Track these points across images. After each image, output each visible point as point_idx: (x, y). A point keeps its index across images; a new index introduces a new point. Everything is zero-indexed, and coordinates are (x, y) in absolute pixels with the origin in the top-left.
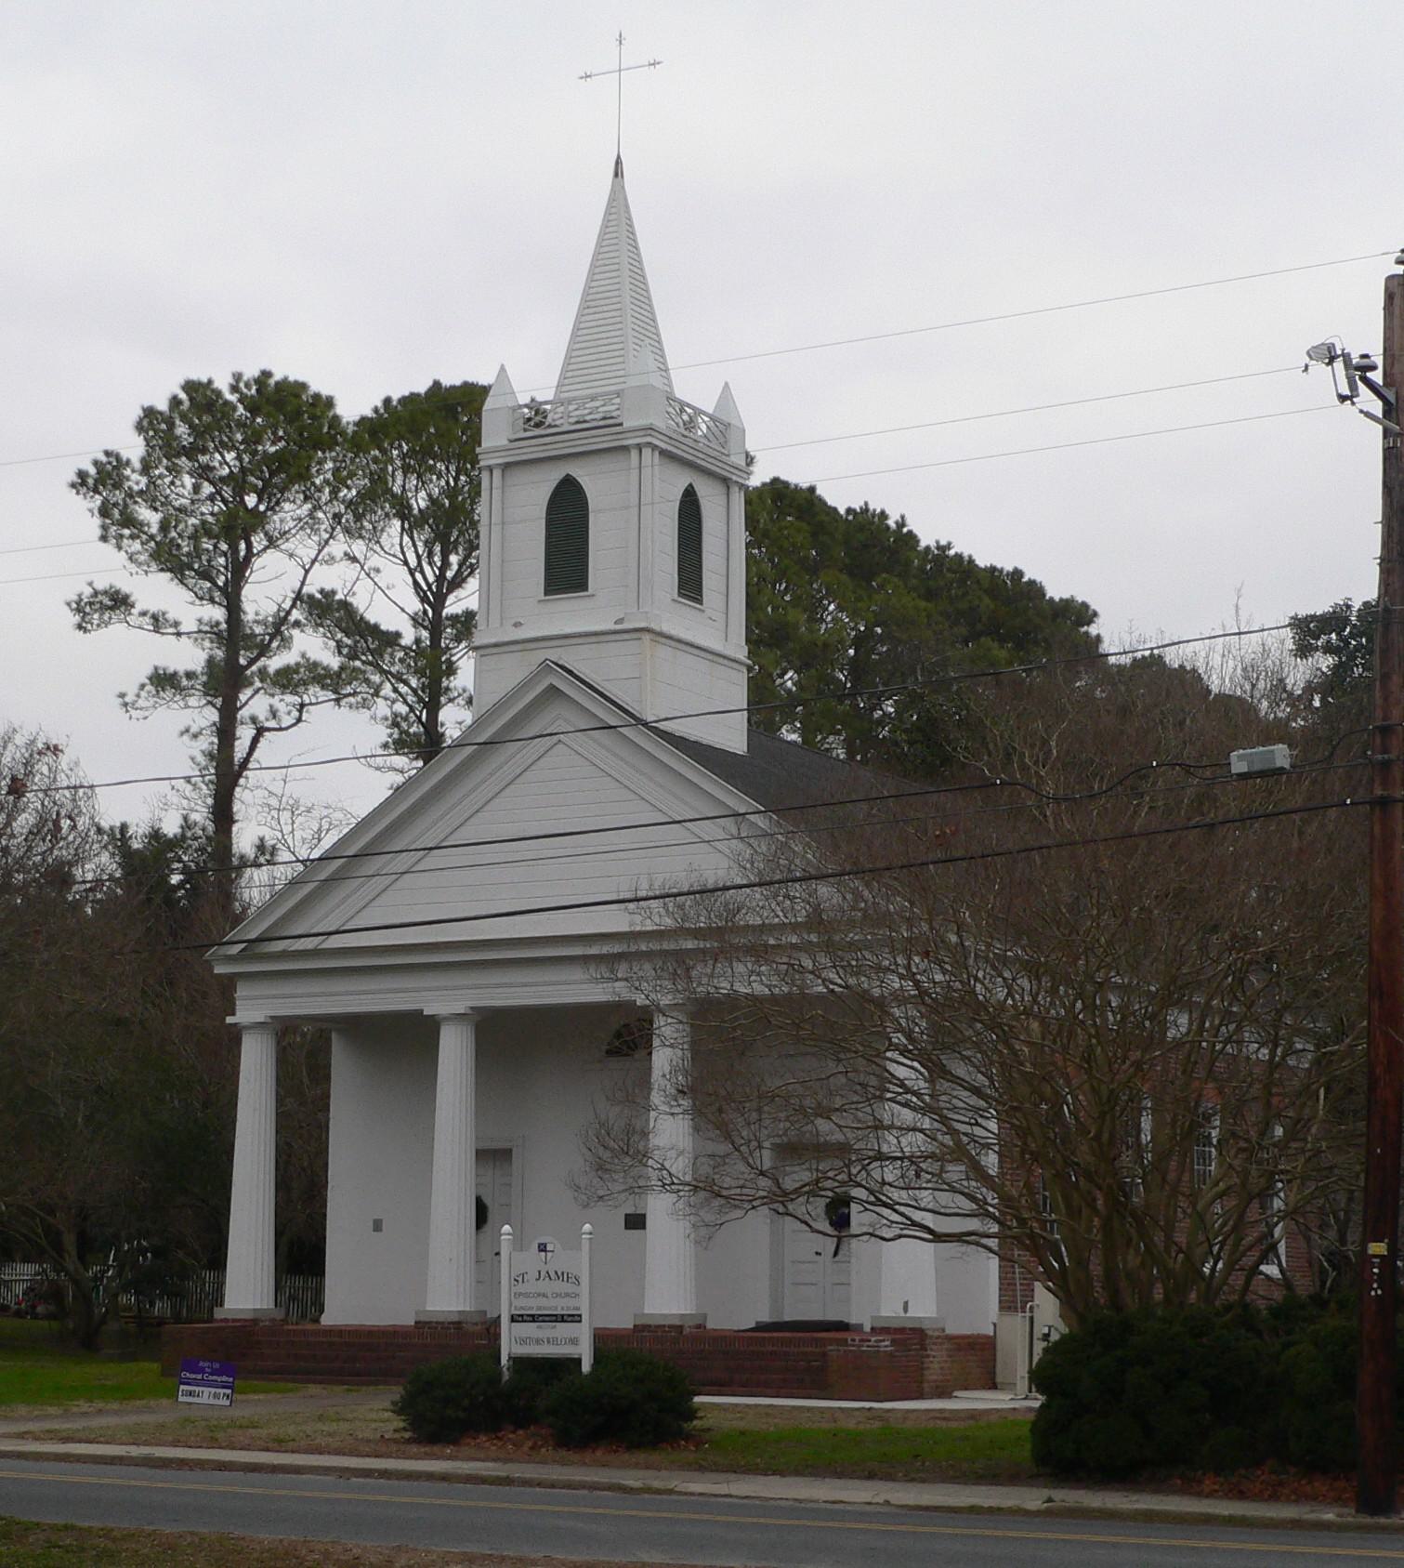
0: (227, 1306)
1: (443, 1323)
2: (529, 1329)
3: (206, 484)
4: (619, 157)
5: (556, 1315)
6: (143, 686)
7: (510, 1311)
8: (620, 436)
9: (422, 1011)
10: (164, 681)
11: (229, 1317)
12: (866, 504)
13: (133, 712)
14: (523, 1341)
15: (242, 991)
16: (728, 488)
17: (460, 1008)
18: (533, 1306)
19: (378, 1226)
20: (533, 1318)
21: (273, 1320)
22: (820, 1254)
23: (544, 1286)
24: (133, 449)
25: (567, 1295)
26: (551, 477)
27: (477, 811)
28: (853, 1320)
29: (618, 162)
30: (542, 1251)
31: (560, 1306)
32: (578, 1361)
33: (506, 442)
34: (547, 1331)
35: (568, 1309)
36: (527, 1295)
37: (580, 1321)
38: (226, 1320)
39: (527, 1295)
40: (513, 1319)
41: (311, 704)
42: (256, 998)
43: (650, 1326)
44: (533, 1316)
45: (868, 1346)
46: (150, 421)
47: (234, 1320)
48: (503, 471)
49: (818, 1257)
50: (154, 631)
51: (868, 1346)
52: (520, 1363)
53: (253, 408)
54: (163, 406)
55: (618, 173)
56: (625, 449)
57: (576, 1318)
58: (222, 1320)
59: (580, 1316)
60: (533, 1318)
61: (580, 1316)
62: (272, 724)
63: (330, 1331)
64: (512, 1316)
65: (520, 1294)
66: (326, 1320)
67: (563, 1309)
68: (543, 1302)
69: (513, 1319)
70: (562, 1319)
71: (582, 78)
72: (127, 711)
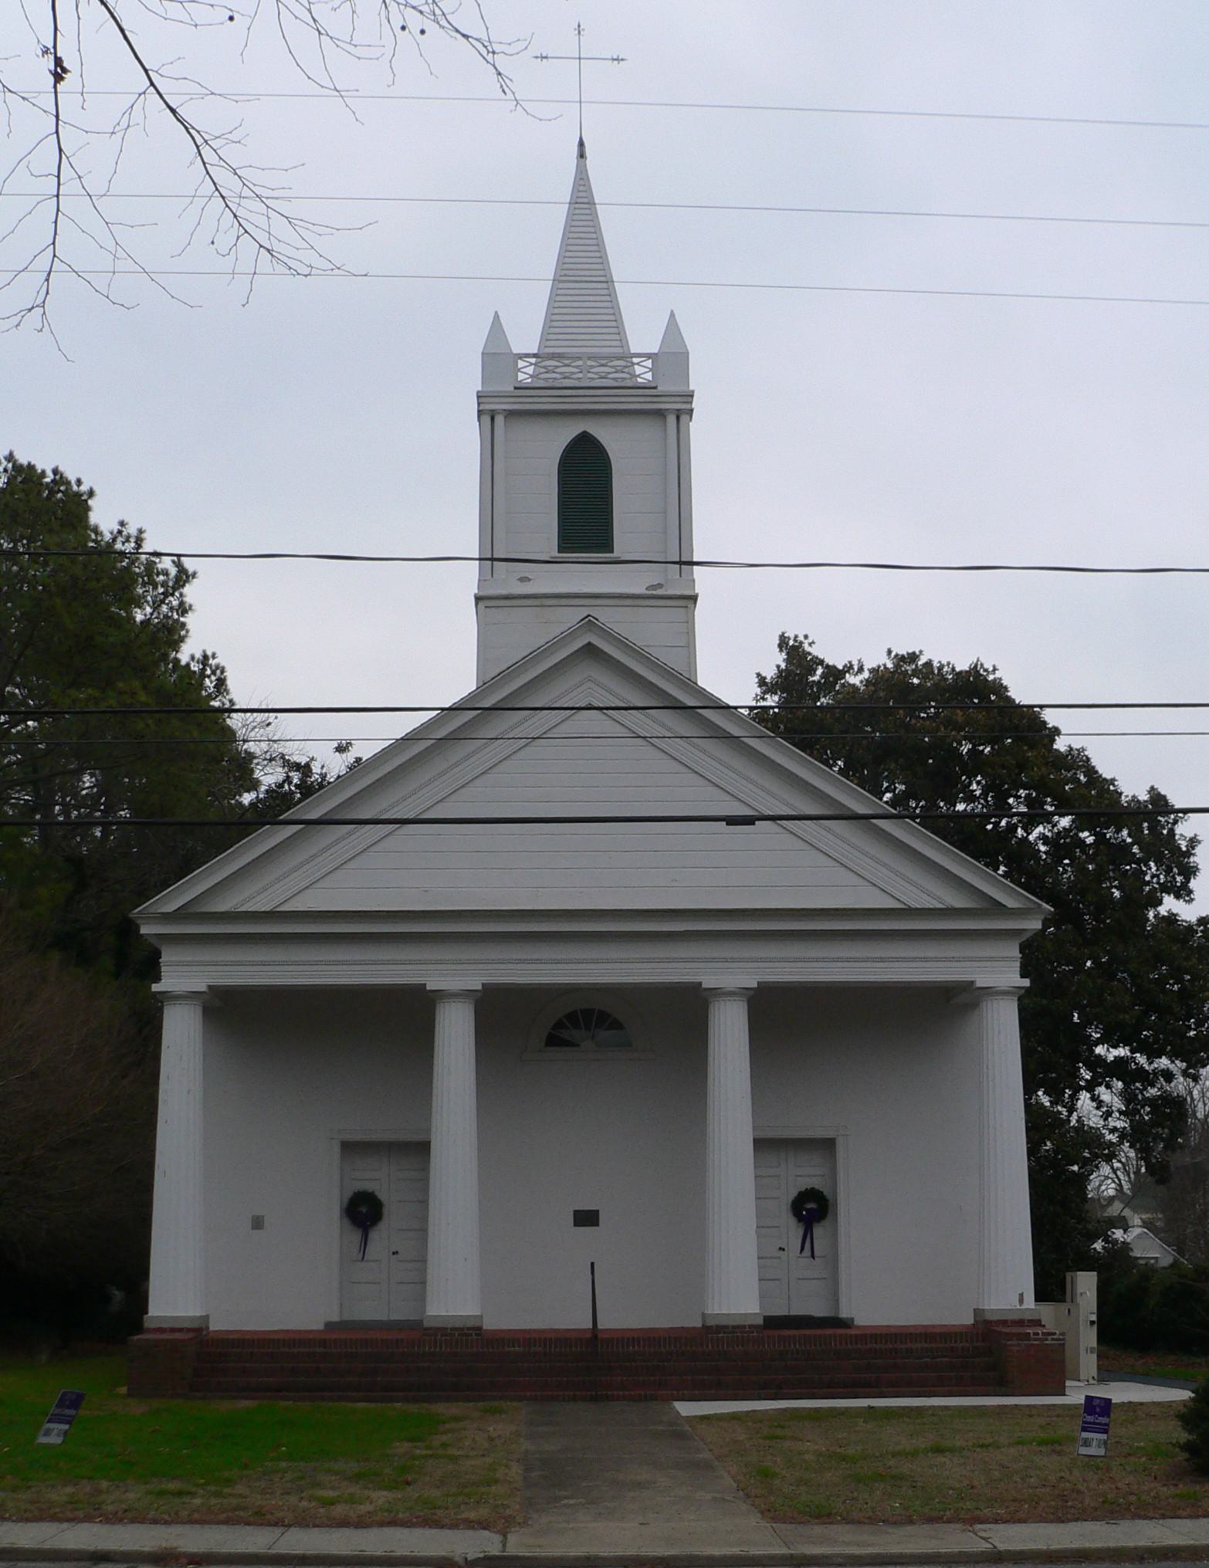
8: (656, 399)
12: (204, 651)
15: (167, 956)
19: (258, 1223)
22: (784, 1250)
26: (564, 434)
28: (844, 1314)
29: (581, 144)
33: (513, 389)
42: (189, 964)
43: (726, 1327)
45: (1053, 1339)
48: (505, 417)
49: (782, 1252)
51: (1053, 1339)
55: (582, 155)
56: (661, 414)
71: (537, 57)
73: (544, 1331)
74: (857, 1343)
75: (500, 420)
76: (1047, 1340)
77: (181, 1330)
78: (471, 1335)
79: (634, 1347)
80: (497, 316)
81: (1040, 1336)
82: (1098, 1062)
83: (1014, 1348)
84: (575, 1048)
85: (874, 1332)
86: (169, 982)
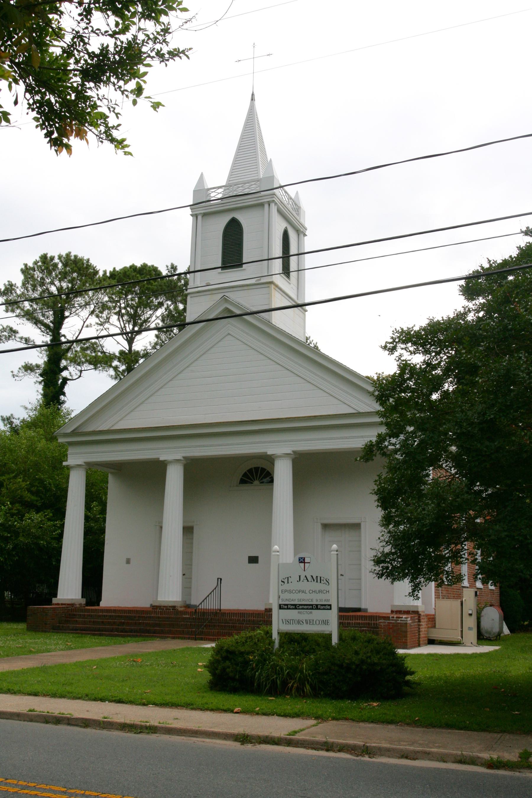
0: (59, 597)
1: (167, 607)
2: (293, 614)
3: (89, 109)
4: (253, 92)
5: (312, 605)
6: (20, 369)
7: (278, 602)
9: (159, 458)
10: (28, 368)
11: (60, 602)
13: (16, 378)
14: (288, 622)
15: (71, 451)
16: (298, 235)
17: (179, 456)
18: (296, 598)
19: (128, 561)
20: (295, 607)
21: (80, 604)
23: (304, 585)
24: (18, 279)
25: (320, 591)
26: (224, 220)
27: (188, 367)
28: (363, 607)
30: (301, 562)
31: (316, 599)
32: (329, 637)
34: (305, 615)
35: (321, 600)
36: (290, 592)
37: (331, 609)
38: (58, 604)
39: (290, 592)
40: (281, 607)
41: (85, 370)
44: (295, 605)
45: (401, 620)
46: (26, 271)
47: (62, 604)
49: (342, 576)
50: (25, 343)
52: (283, 635)
53: (65, 265)
54: (31, 264)
55: (253, 99)
56: (262, 205)
57: (330, 607)
58: (56, 604)
59: (330, 605)
60: (295, 607)
61: (330, 605)
62: (70, 378)
63: (108, 610)
64: (280, 605)
65: (286, 591)
66: (103, 604)
67: (317, 600)
68: (301, 596)
69: (281, 607)
70: (317, 607)
72: (14, 377)
73: (234, 610)
74: (125, 613)
75: (200, 218)
76: (398, 620)
77: (65, 604)
78: (170, 609)
79: (234, 617)
80: (202, 174)
81: (395, 618)
82: (430, 485)
83: (382, 624)
84: (251, 485)
85: (115, 609)
86: (71, 461)
